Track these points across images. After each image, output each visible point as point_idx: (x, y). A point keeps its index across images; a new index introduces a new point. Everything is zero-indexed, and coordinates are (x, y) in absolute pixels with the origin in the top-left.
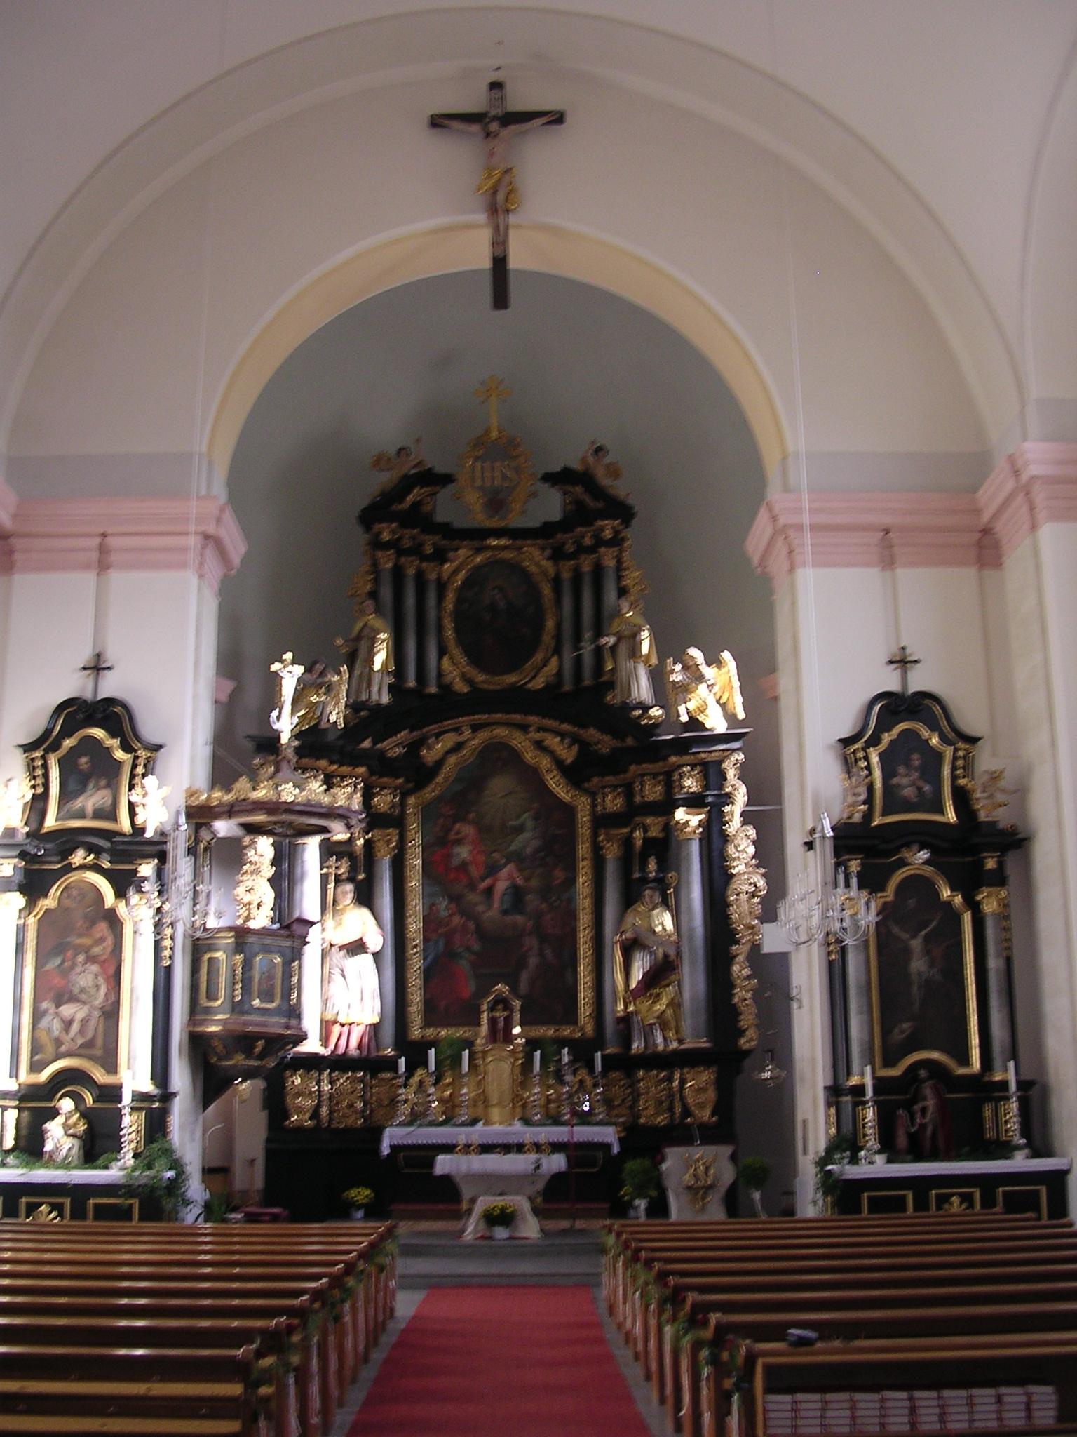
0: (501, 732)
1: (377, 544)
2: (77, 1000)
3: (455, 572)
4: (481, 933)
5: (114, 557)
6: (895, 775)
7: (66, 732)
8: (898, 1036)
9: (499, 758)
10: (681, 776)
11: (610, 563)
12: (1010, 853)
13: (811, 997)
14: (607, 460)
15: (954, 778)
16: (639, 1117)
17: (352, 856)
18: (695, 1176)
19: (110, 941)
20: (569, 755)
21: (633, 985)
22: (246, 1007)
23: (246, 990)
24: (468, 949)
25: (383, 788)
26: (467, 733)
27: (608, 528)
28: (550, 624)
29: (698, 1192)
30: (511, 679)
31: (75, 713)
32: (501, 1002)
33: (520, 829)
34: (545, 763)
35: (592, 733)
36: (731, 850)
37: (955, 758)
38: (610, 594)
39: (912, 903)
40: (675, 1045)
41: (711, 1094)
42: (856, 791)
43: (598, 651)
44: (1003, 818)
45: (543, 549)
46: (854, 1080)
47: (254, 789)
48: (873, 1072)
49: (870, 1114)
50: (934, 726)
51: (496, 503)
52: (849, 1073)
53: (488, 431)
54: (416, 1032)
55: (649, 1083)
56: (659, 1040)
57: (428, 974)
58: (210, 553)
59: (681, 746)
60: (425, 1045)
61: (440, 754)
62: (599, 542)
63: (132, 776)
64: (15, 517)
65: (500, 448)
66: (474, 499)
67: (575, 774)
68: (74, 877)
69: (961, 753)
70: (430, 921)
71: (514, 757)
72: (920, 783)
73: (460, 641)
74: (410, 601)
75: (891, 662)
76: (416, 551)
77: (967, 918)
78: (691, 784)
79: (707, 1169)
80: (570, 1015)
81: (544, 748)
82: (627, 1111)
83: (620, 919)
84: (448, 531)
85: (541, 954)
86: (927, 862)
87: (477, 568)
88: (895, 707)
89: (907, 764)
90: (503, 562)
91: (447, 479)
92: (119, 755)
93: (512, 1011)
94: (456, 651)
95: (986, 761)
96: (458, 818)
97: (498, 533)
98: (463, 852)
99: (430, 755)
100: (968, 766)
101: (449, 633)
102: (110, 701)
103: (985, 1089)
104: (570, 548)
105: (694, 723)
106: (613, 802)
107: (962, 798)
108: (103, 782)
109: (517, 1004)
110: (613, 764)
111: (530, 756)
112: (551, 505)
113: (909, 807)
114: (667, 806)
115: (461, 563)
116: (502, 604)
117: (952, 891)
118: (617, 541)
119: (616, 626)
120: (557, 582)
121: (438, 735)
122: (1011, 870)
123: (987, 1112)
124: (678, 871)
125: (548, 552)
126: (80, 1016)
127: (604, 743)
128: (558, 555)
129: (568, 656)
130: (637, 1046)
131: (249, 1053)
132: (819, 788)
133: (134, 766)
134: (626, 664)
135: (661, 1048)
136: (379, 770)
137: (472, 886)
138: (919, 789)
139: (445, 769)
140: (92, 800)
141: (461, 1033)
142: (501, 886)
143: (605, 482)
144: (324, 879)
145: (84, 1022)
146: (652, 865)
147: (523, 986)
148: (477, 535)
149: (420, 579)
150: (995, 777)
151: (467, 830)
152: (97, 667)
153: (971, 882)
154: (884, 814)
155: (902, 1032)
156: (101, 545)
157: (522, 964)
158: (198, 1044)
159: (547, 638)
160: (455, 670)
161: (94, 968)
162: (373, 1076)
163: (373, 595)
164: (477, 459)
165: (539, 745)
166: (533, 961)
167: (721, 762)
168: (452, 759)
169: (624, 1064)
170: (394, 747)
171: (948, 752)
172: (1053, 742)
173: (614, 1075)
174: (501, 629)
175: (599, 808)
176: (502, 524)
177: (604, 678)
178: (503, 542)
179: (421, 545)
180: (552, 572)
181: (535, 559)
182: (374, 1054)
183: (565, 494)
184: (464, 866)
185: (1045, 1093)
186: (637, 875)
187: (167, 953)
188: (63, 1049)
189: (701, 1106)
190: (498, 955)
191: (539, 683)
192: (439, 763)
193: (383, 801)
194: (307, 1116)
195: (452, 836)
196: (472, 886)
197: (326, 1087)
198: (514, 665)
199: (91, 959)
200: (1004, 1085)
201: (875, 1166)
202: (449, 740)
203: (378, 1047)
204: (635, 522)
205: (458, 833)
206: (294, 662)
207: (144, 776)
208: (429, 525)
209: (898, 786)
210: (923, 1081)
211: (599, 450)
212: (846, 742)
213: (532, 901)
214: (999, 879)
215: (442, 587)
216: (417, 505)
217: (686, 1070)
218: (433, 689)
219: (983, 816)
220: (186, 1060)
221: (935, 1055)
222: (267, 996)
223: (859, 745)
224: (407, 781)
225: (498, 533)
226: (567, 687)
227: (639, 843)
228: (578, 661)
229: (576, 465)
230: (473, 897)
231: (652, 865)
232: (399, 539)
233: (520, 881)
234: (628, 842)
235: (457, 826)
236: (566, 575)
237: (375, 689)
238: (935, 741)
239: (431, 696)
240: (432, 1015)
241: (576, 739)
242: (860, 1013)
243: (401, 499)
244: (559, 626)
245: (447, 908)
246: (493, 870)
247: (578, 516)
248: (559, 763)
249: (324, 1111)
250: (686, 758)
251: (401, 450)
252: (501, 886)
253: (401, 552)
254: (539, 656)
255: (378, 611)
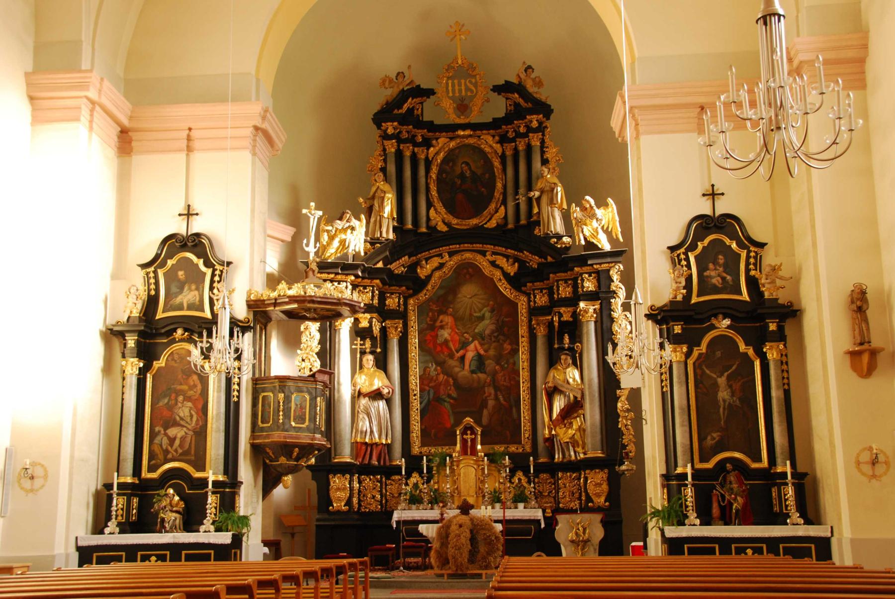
0: (468, 255)
1: (385, 137)
2: (179, 425)
3: (437, 153)
4: (457, 386)
5: (196, 144)
6: (707, 269)
7: (170, 256)
8: (709, 442)
9: (468, 272)
10: (583, 280)
11: (536, 143)
12: (787, 321)
13: (652, 415)
14: (533, 76)
15: (747, 270)
16: (559, 503)
17: (373, 339)
18: (577, 534)
19: (199, 387)
20: (512, 270)
21: (555, 416)
22: (287, 426)
23: (287, 416)
24: (449, 396)
25: (392, 294)
26: (447, 257)
27: (534, 120)
28: (499, 185)
29: (581, 544)
30: (474, 221)
31: (174, 244)
32: (468, 429)
33: (482, 318)
34: (498, 274)
35: (526, 255)
36: (615, 327)
37: (748, 257)
38: (537, 163)
39: (718, 354)
40: (582, 456)
41: (605, 487)
42: (679, 280)
43: (530, 201)
44: (783, 298)
45: (493, 136)
46: (679, 470)
47: (289, 289)
48: (693, 466)
49: (689, 492)
50: (733, 236)
51: (462, 107)
52: (676, 466)
53: (456, 59)
54: (416, 450)
55: (565, 480)
56: (572, 453)
57: (423, 412)
58: (260, 139)
59: (582, 261)
60: (420, 458)
61: (429, 272)
62: (530, 129)
63: (212, 282)
64: (131, 118)
65: (465, 71)
66: (448, 105)
67: (515, 282)
68: (175, 347)
69: (752, 254)
70: (424, 379)
71: (478, 271)
72: (725, 275)
73: (441, 199)
74: (408, 173)
75: (704, 195)
76: (412, 140)
77: (757, 364)
78: (589, 285)
79: (585, 529)
80: (516, 438)
81: (496, 264)
82: (552, 500)
83: (547, 375)
84: (432, 127)
85: (496, 398)
86: (728, 327)
87: (451, 151)
88: (705, 224)
89: (715, 262)
90: (469, 145)
91: (430, 92)
92: (203, 268)
93: (476, 434)
94: (439, 205)
95: (769, 258)
96: (441, 312)
97: (464, 127)
98: (445, 334)
99: (422, 273)
100: (758, 264)
101: (434, 193)
102: (198, 235)
103: (771, 478)
104: (511, 135)
105: (590, 245)
106: (541, 300)
107: (753, 283)
108: (193, 287)
109: (479, 430)
110: (540, 274)
111: (487, 270)
112: (499, 107)
113: (715, 290)
114: (573, 301)
115: (441, 146)
116: (468, 174)
117: (746, 345)
118: (541, 129)
119: (540, 185)
120: (503, 158)
121: (427, 260)
122: (788, 331)
123: (774, 491)
124: (581, 342)
125: (497, 138)
126: (179, 436)
127: (534, 261)
128: (503, 140)
129: (511, 204)
130: (558, 457)
131: (289, 456)
132: (656, 278)
133: (213, 275)
134: (545, 208)
135: (573, 457)
136: (390, 280)
137: (451, 356)
138: (723, 279)
139: (433, 281)
140: (188, 296)
141: (446, 449)
142: (470, 355)
143: (531, 88)
144: (353, 352)
145: (183, 439)
146: (567, 339)
147: (485, 420)
148: (451, 128)
149: (414, 158)
150: (775, 269)
151: (448, 319)
152: (189, 214)
153: (758, 340)
154: (698, 296)
155: (714, 439)
156: (188, 136)
157: (484, 404)
158: (257, 450)
159: (497, 195)
160: (439, 218)
161: (190, 404)
162: (388, 478)
163: (383, 170)
164: (448, 78)
165: (493, 264)
166: (491, 403)
167: (609, 271)
168: (437, 274)
169: (552, 469)
170: (398, 267)
171: (744, 254)
172: (814, 244)
173: (544, 476)
174: (467, 189)
175: (532, 303)
176: (467, 121)
177: (535, 218)
178: (467, 132)
179: (414, 136)
180: (500, 151)
181: (489, 142)
182: (388, 464)
183: (507, 99)
184: (446, 342)
185: (815, 482)
186: (556, 346)
187: (236, 393)
188: (170, 456)
189: (598, 495)
190: (468, 399)
191: (493, 224)
192: (429, 277)
193: (392, 302)
194: (343, 504)
195: (438, 324)
196: (451, 356)
197: (356, 485)
198: (477, 213)
199: (188, 399)
200: (784, 475)
201: (694, 529)
202: (435, 262)
203: (391, 460)
204: (552, 116)
205: (441, 322)
206: (317, 208)
207: (219, 282)
208: (419, 123)
209: (710, 277)
210: (728, 472)
211: (529, 68)
212: (672, 249)
213: (490, 364)
214: (780, 336)
215: (428, 163)
216: (411, 111)
217: (587, 472)
218: (424, 230)
219: (767, 295)
220: (248, 462)
221: (737, 455)
222: (301, 419)
223: (683, 250)
224: (408, 288)
225: (464, 127)
226: (510, 226)
227: (556, 324)
228: (517, 206)
229: (515, 80)
230: (452, 363)
231: (567, 339)
232: (400, 132)
233: (482, 352)
234: (551, 324)
235: (441, 317)
236: (509, 153)
237: (384, 230)
238: (734, 245)
239: (424, 233)
240: (426, 438)
241: (516, 260)
242: (682, 426)
243: (400, 107)
244: (505, 187)
245: (435, 370)
246: (464, 345)
247: (516, 114)
248: (506, 275)
249: (355, 500)
250: (585, 269)
251: (398, 74)
252: (470, 355)
253: (400, 141)
254: (493, 206)
255: (386, 179)
